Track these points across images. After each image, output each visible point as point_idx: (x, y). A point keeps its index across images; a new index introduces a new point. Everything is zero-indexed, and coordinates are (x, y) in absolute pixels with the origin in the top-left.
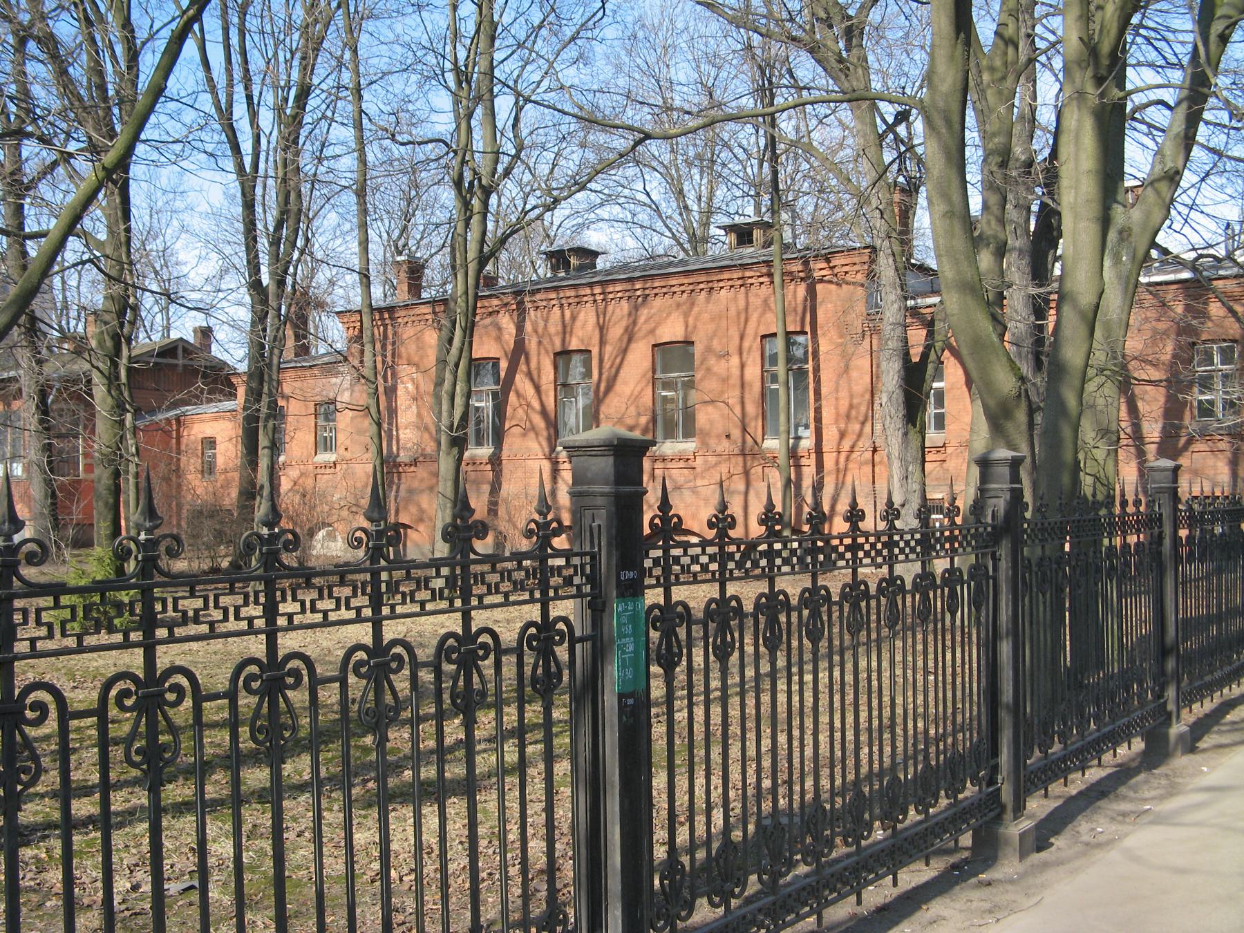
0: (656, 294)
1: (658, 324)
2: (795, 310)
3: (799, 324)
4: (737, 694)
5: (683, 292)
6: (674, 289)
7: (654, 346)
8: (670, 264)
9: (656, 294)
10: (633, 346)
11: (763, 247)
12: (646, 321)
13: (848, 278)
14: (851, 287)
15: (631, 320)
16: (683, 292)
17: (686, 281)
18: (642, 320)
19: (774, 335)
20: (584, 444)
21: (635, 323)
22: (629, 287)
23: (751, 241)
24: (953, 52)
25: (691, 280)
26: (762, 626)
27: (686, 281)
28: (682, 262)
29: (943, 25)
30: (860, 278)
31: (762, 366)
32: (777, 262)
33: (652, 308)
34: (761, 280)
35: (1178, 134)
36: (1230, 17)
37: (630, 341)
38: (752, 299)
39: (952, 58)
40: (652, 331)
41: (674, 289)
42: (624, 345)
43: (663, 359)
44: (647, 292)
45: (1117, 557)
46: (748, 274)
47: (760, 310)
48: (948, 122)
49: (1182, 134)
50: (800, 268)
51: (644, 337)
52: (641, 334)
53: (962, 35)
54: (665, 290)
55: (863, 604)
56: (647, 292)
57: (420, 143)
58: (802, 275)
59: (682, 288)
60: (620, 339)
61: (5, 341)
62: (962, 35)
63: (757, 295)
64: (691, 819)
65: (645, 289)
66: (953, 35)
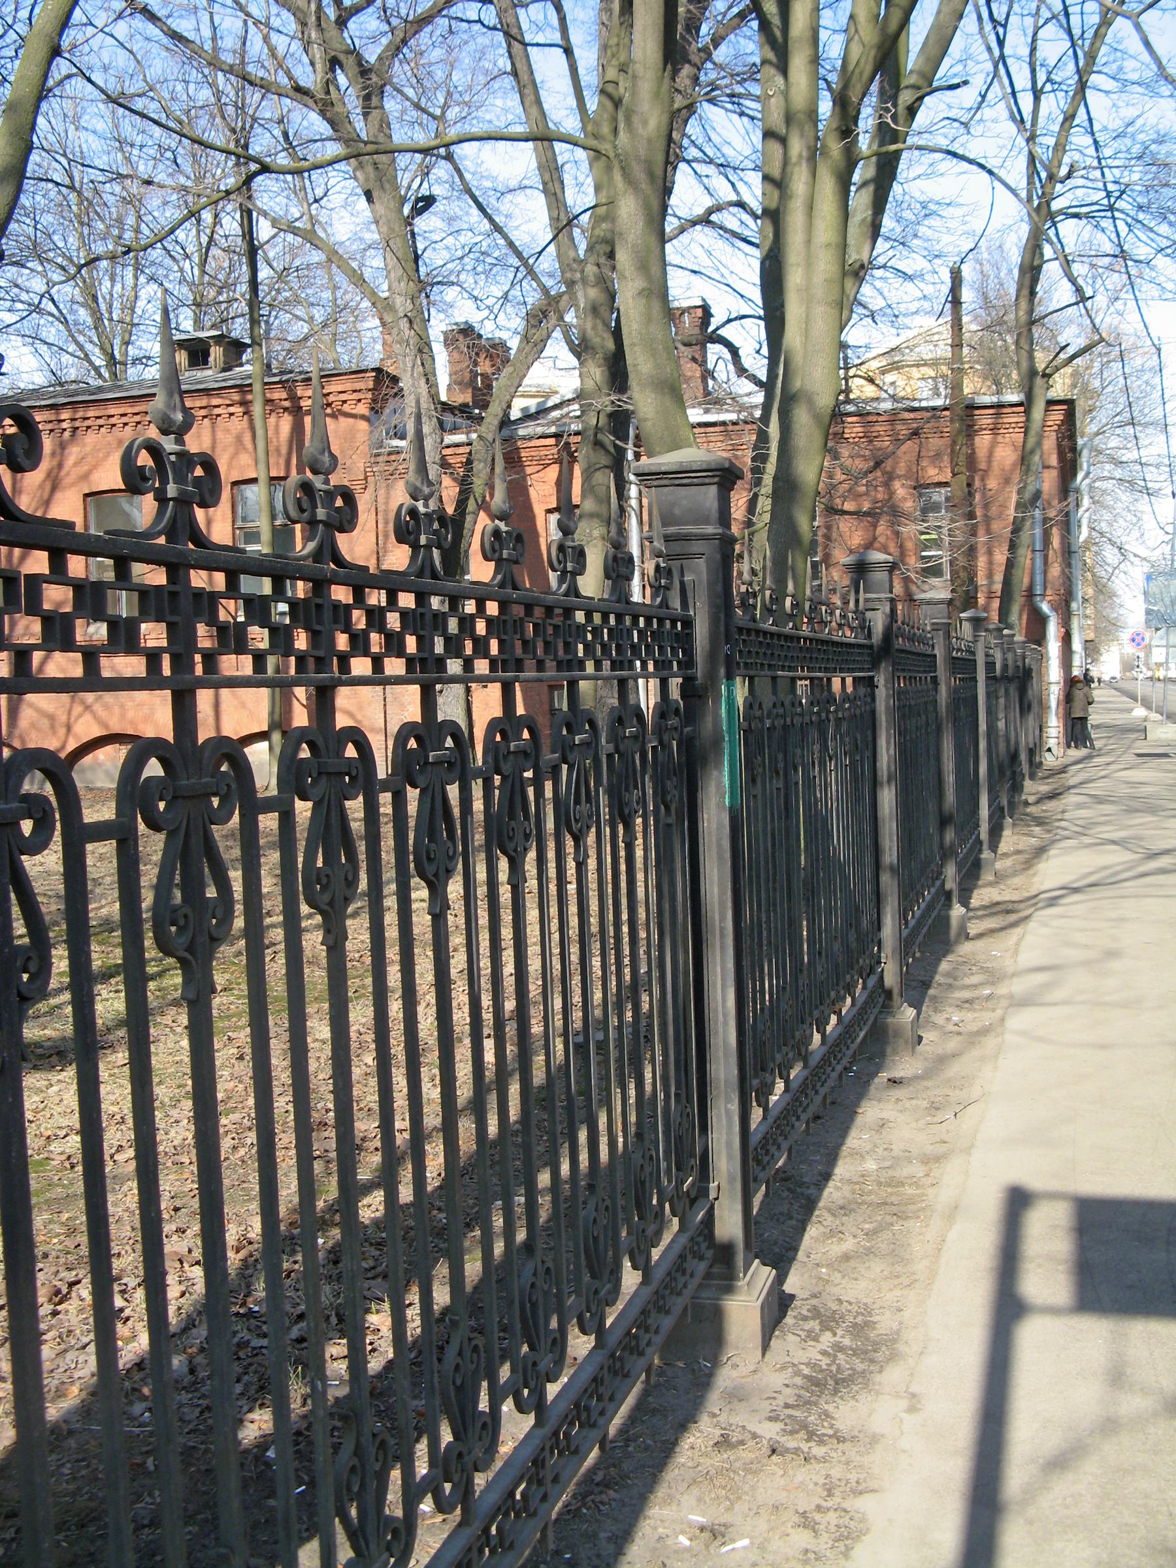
0: (88, 427)
1: (95, 467)
2: (278, 450)
3: (283, 467)
4: (317, 927)
5: (125, 424)
6: (113, 421)
7: (86, 495)
8: (84, 392)
9: (88, 427)
10: (58, 495)
11: (224, 370)
12: (76, 464)
13: (346, 408)
14: (351, 420)
15: (55, 463)
16: (125, 424)
17: (130, 410)
18: (70, 461)
19: (254, 481)
20: (674, 468)
21: (60, 466)
22: (53, 418)
23: (206, 362)
24: (659, 87)
25: (136, 410)
26: (149, 875)
27: (130, 410)
28: (100, 389)
29: (649, 52)
30: (362, 409)
31: (234, 522)
32: (257, 387)
33: (84, 445)
34: (232, 410)
35: (864, 220)
36: (918, 88)
37: (54, 488)
38: (220, 435)
39: (657, 94)
40: (85, 477)
41: (113, 421)
42: (46, 495)
43: (97, 516)
44: (77, 424)
45: (369, 786)
46: (215, 402)
47: (231, 450)
48: (651, 175)
49: (869, 219)
50: (284, 395)
51: (73, 485)
52: (67, 481)
53: (669, 67)
54: (101, 422)
55: (453, 791)
56: (77, 424)
57: (131, 52)
58: (287, 404)
59: (125, 419)
60: (41, 487)
61: (274, 9)
62: (669, 67)
63: (227, 431)
64: (547, 1047)
65: (73, 420)
66: (661, 65)
